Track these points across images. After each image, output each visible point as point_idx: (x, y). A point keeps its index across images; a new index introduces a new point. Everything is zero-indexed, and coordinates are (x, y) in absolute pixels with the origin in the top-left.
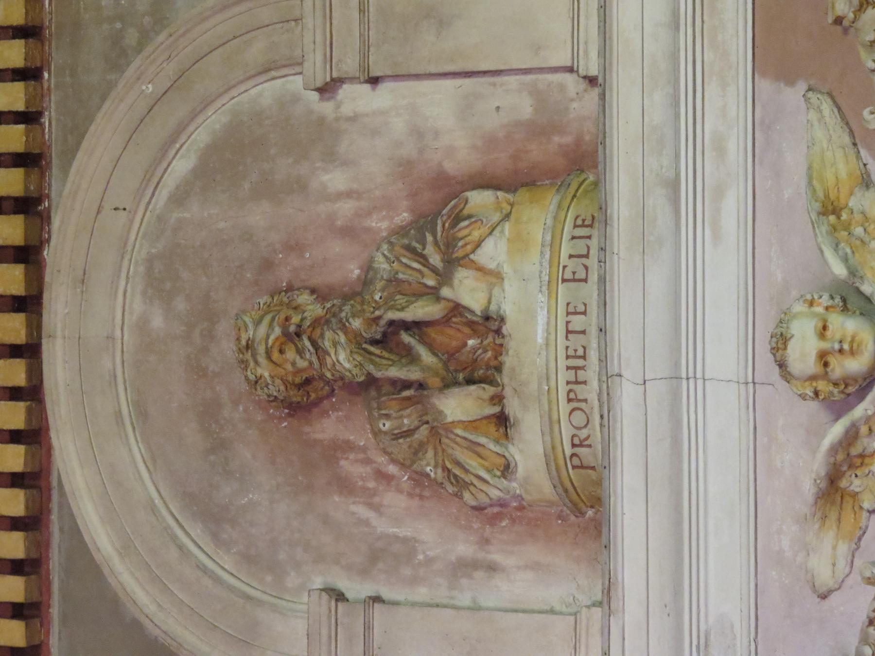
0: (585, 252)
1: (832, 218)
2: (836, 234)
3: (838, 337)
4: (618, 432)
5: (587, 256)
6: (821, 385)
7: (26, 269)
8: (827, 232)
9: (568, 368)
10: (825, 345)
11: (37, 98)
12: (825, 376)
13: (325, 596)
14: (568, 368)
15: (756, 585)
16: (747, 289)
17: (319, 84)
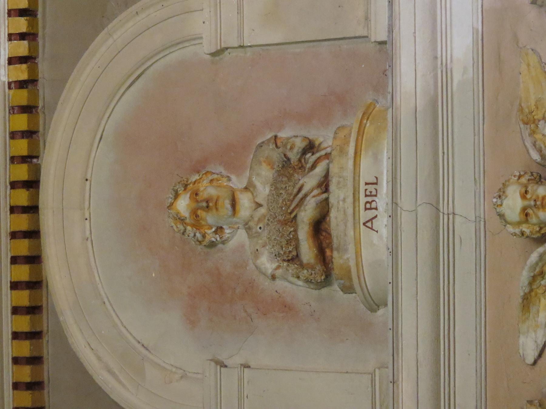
0: (375, 181)
1: (533, 126)
2: (535, 136)
3: (534, 197)
10: (526, 203)
11: (34, 48)
12: (527, 221)
13: (213, 364)
15: (482, 6)
16: (478, 54)
17: (213, 50)
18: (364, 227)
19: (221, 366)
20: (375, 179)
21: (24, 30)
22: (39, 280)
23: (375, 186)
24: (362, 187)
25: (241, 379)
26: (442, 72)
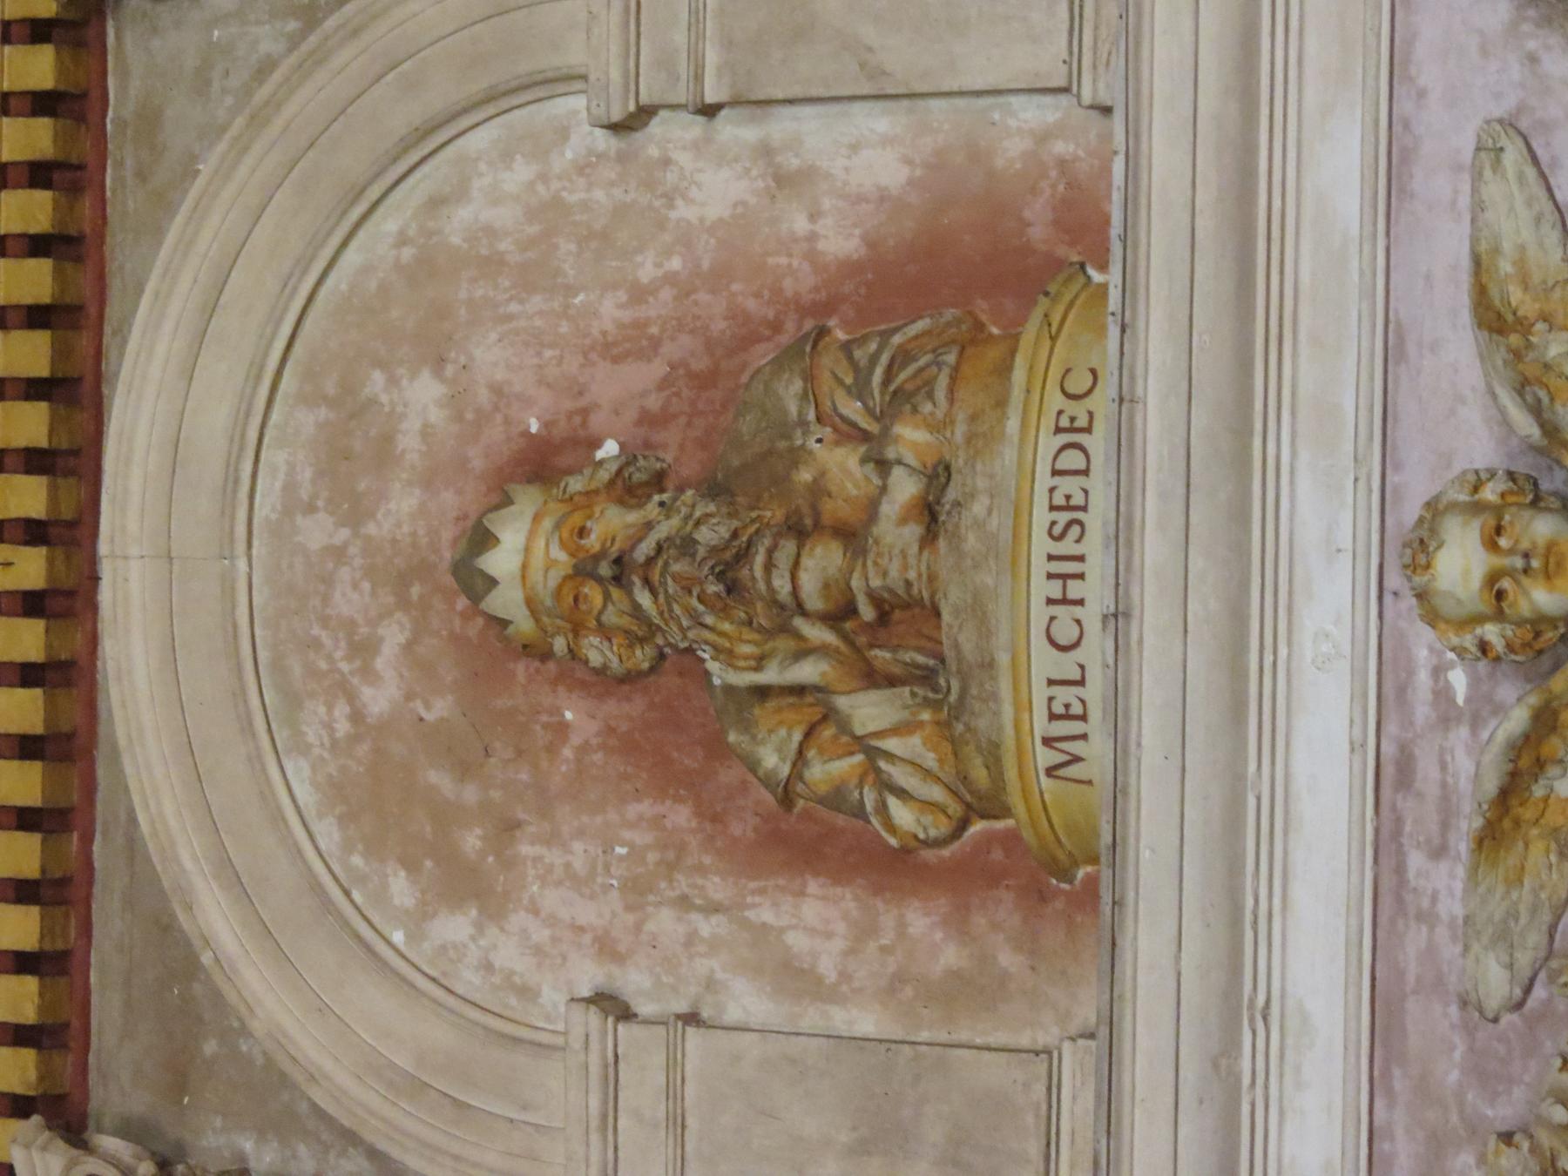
0: (1078, 677)
4: (1128, 1012)
5: (1081, 683)
6: (1491, 632)
7: (44, 841)
8: (1505, 362)
9: (1050, 576)
12: (1499, 616)
14: (1050, 576)
17: (616, 115)
18: (1046, 750)
19: (618, 1019)
20: (1079, 671)
21: (28, 1014)
22: (62, 805)
23: (1081, 480)
24: (1040, 693)
25: (674, 1064)
26: (1253, 1105)
